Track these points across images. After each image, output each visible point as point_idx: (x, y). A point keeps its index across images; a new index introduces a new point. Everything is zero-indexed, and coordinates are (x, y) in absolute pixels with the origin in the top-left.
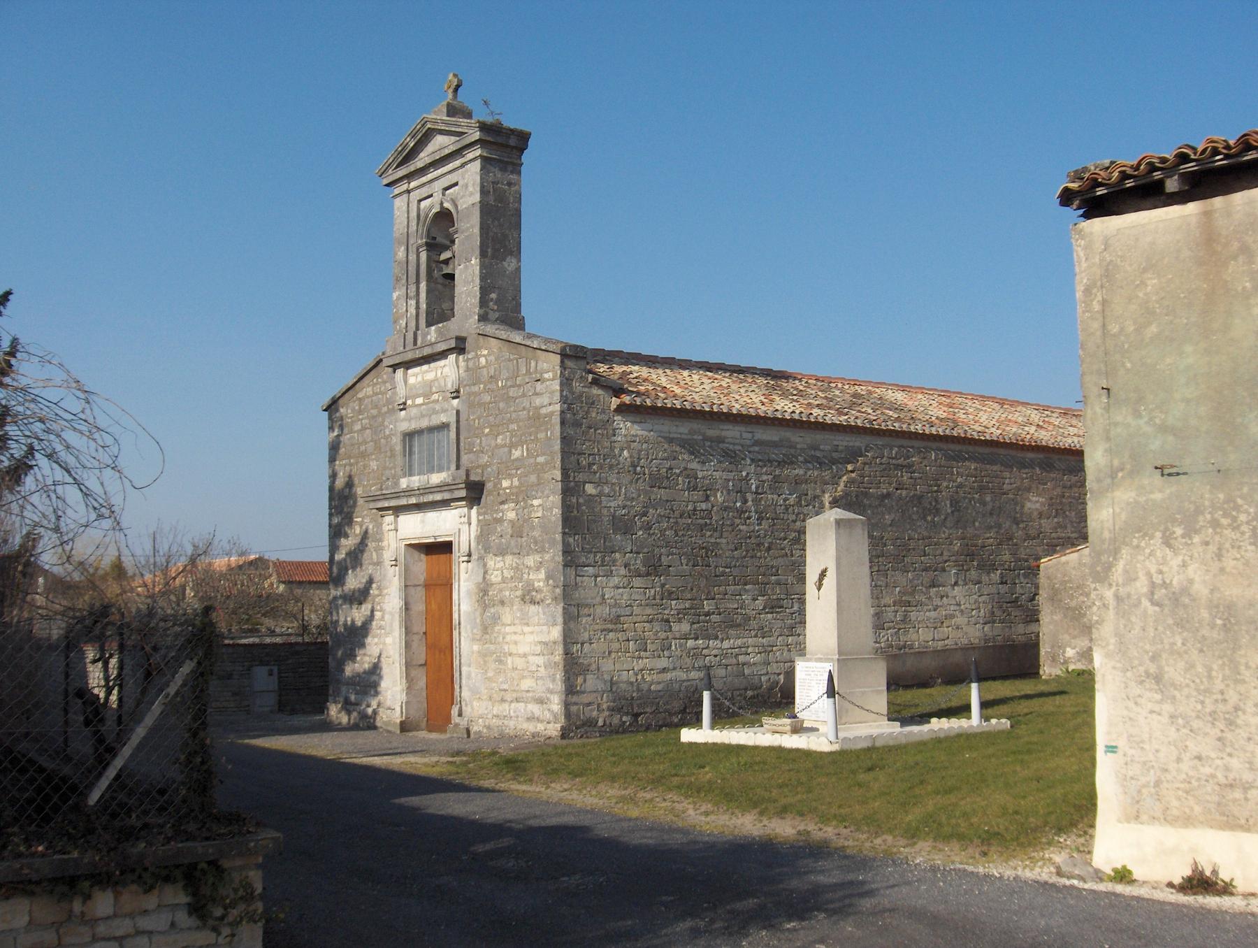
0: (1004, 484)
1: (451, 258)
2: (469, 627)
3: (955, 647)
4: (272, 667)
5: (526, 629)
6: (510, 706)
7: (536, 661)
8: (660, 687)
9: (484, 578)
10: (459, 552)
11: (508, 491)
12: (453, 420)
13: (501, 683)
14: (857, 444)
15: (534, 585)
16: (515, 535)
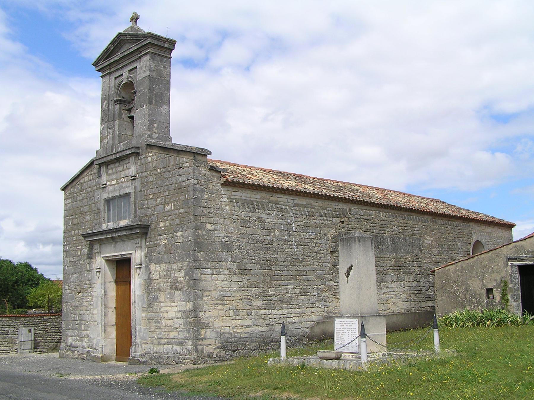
0: (414, 230)
1: (132, 108)
2: (140, 303)
3: (393, 313)
4: (31, 328)
5: (173, 304)
6: (163, 346)
7: (179, 322)
8: (246, 336)
9: (149, 276)
10: (135, 262)
11: (163, 228)
12: (132, 191)
13: (159, 334)
14: (345, 208)
15: (177, 279)
16: (167, 252)
